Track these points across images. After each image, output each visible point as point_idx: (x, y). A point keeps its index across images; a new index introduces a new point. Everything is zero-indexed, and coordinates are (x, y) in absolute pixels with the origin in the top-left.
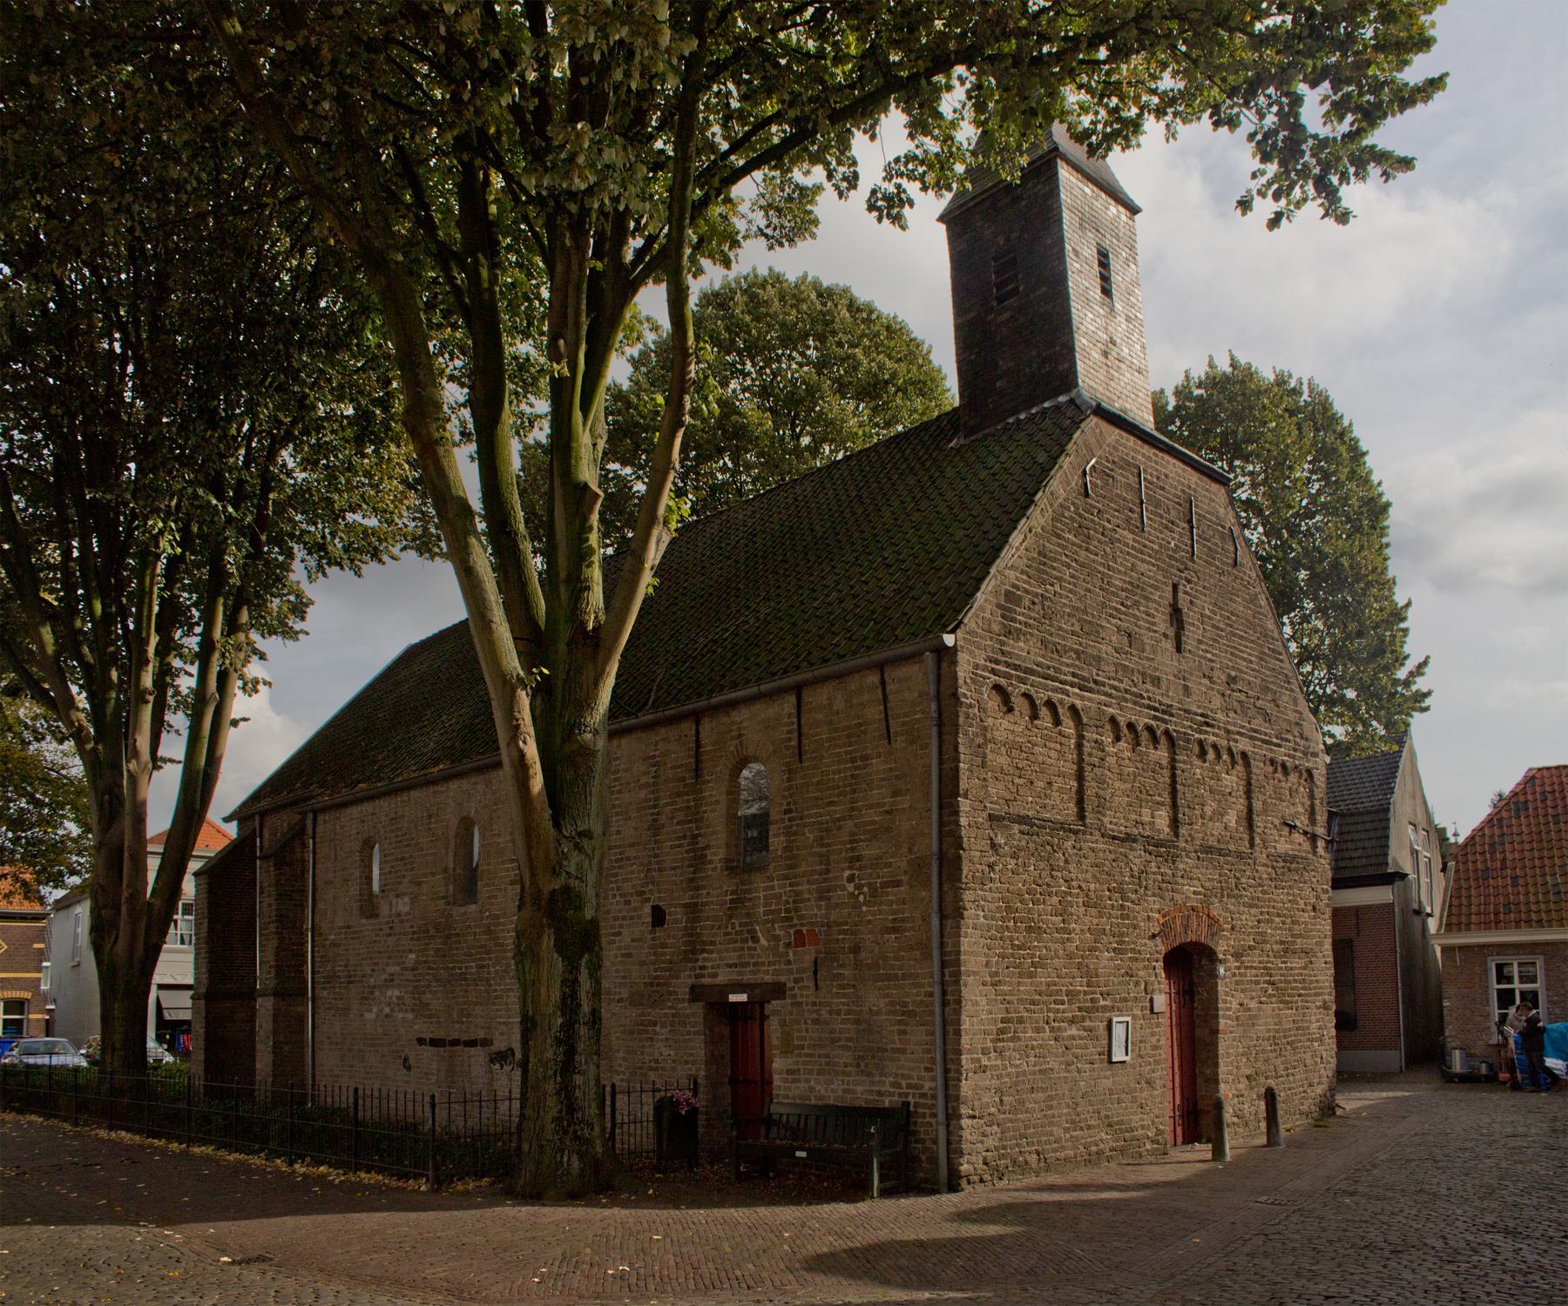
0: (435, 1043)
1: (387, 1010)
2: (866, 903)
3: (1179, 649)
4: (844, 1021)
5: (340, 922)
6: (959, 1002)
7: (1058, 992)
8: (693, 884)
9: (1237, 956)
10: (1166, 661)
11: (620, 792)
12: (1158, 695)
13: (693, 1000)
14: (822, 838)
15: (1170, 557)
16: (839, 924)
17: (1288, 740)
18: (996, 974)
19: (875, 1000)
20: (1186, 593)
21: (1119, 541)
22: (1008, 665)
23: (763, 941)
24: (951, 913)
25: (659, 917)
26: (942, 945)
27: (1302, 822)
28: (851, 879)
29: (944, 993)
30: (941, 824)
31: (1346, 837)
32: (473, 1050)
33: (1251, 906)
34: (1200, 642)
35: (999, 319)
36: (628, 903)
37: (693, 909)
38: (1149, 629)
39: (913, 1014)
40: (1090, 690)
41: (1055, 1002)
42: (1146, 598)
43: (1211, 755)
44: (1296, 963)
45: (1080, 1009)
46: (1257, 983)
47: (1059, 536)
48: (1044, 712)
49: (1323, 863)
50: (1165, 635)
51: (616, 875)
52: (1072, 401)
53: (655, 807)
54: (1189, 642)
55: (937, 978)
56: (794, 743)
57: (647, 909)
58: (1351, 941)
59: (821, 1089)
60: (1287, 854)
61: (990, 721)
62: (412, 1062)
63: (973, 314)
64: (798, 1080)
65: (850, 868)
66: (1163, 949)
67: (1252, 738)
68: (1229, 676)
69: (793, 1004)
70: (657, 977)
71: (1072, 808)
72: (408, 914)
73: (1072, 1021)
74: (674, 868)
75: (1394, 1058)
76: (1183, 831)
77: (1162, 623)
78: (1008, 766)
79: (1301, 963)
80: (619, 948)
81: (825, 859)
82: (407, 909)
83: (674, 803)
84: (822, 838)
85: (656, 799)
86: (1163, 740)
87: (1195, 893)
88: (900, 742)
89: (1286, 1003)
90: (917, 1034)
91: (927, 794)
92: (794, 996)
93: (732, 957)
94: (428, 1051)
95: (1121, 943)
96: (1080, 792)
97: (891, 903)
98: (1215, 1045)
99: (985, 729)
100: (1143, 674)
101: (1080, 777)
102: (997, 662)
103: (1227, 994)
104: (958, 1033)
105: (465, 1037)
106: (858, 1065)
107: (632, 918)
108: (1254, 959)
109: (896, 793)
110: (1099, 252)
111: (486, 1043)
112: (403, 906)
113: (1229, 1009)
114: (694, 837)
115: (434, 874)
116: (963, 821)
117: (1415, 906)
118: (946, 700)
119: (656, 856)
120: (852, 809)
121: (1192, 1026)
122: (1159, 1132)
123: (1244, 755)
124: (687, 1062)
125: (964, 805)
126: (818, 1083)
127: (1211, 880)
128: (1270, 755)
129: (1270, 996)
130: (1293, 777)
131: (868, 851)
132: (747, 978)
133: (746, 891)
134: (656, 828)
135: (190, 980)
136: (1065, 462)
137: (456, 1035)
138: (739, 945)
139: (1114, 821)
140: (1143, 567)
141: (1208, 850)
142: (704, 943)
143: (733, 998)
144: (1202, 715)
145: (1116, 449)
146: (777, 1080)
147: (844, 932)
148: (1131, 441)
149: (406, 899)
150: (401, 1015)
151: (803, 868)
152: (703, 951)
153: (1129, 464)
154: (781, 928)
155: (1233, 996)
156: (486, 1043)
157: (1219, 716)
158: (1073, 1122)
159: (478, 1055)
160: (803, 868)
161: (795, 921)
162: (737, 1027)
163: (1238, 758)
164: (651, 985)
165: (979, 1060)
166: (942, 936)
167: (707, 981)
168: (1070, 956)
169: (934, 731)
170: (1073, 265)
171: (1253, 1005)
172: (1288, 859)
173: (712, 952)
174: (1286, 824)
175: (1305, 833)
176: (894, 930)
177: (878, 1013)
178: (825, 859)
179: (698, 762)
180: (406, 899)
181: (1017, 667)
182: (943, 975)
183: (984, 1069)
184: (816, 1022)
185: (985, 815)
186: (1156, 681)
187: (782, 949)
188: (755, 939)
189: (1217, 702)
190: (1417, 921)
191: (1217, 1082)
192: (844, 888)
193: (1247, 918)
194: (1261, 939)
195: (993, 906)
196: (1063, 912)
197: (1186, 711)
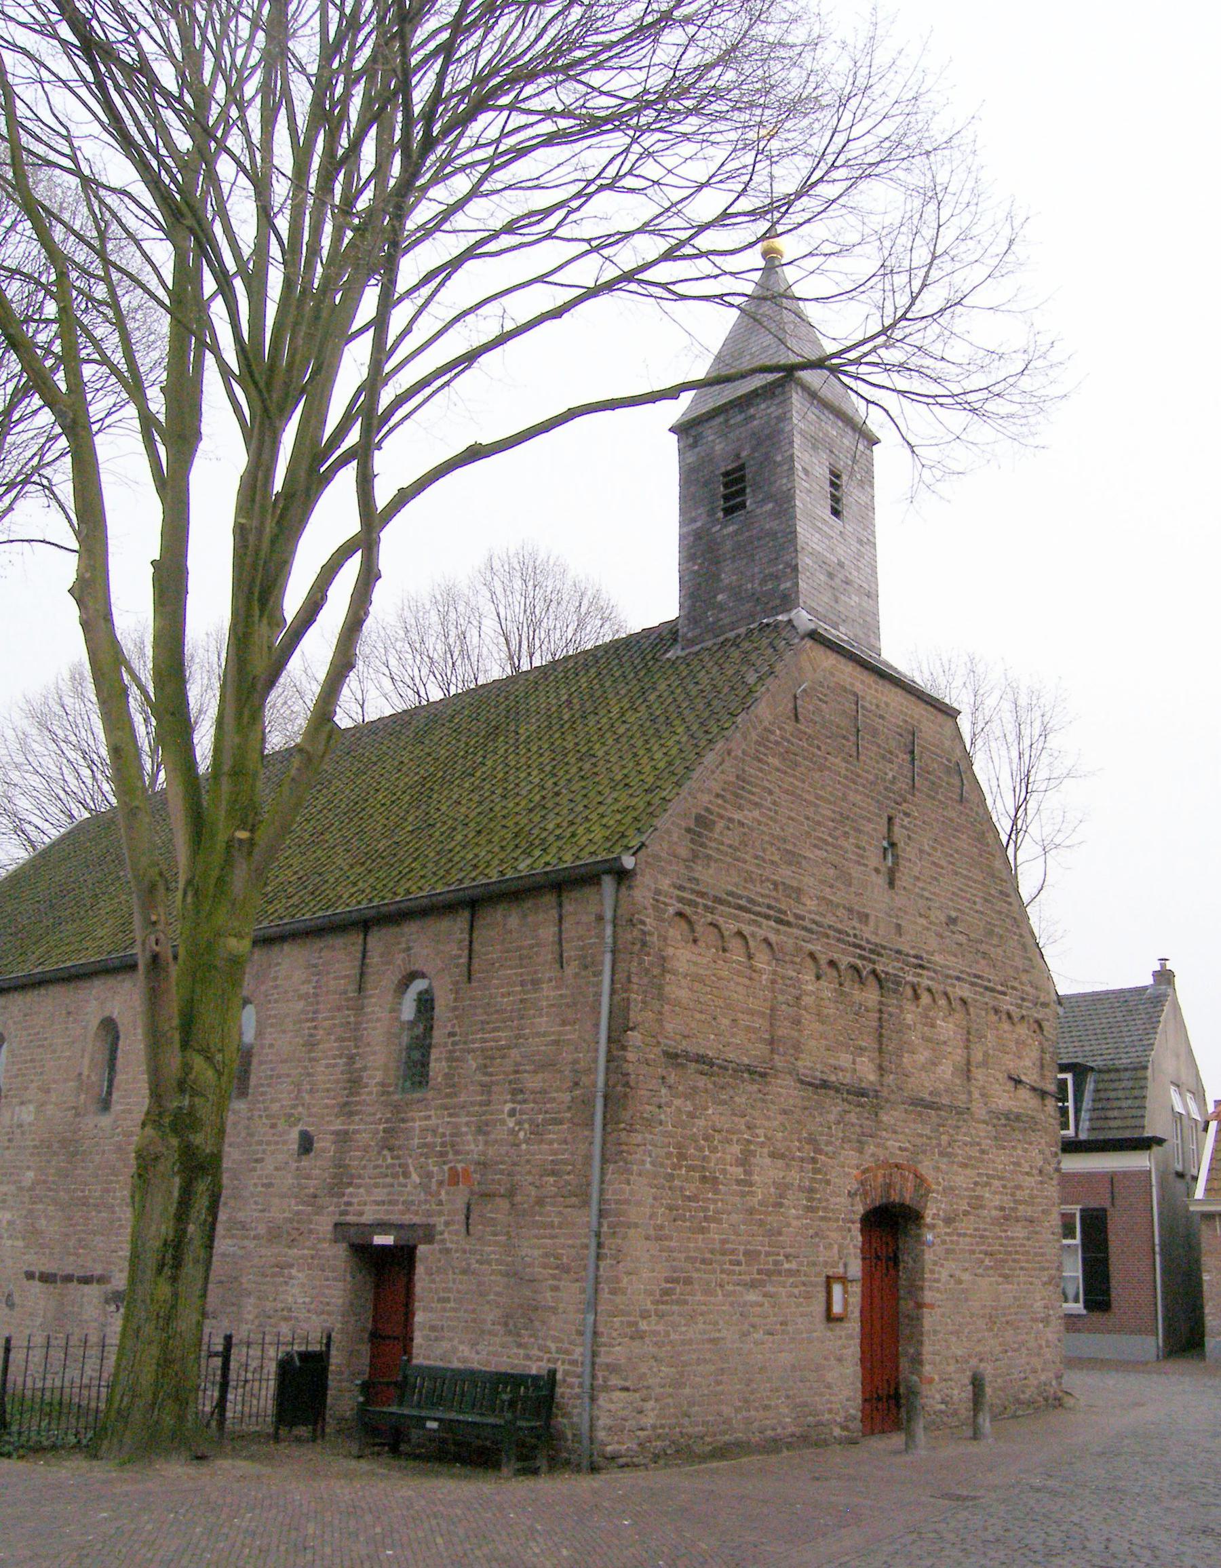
0: (46, 1278)
2: (527, 1141)
3: (891, 884)
4: (493, 1272)
7: (733, 1252)
8: (347, 1110)
9: (948, 1221)
10: (877, 898)
11: (276, 1001)
12: (867, 932)
14: (486, 1066)
15: (886, 789)
16: (497, 1163)
17: (1013, 988)
18: (661, 1227)
20: (903, 827)
21: (829, 769)
22: (693, 891)
23: (415, 1178)
25: (306, 1144)
26: (602, 1192)
28: (512, 1113)
29: (600, 1245)
31: (1102, 1095)
33: (965, 1166)
34: (917, 879)
35: (725, 532)
36: (273, 1126)
37: (343, 1138)
38: (859, 863)
39: (566, 1269)
40: (788, 924)
41: (731, 1263)
42: (857, 830)
43: (925, 999)
44: (1018, 1232)
45: (760, 1272)
46: (972, 1252)
47: (760, 761)
50: (877, 870)
51: (263, 1094)
52: (790, 621)
53: (313, 1020)
54: (903, 880)
55: (595, 1227)
56: (464, 960)
57: (294, 1134)
58: (1104, 1210)
59: (465, 1350)
60: (1010, 1112)
61: (670, 951)
62: (17, 1299)
63: (699, 524)
64: (452, 1333)
65: (513, 1101)
66: (860, 1209)
67: (973, 984)
68: (949, 917)
69: (441, 1251)
70: (298, 1213)
72: (30, 1124)
73: (753, 1285)
74: (328, 1090)
75: (1152, 1344)
80: (259, 1177)
82: (32, 1118)
83: (333, 1018)
84: (486, 1066)
85: (315, 1012)
87: (900, 1148)
88: (571, 970)
89: (1006, 1276)
91: (597, 1025)
92: (443, 1241)
93: (380, 1194)
94: (37, 1286)
95: (810, 1199)
97: (551, 1143)
98: (919, 1318)
99: (664, 958)
100: (850, 910)
102: (681, 888)
103: (935, 1263)
105: (80, 1273)
106: (506, 1324)
107: (277, 1143)
108: (966, 1225)
109: (564, 1023)
110: (832, 473)
111: (101, 1280)
113: (937, 1280)
114: (351, 1058)
115: (66, 1080)
117: (1179, 1168)
119: (309, 1075)
120: (518, 1037)
123: (964, 1001)
124: (323, 1313)
126: (461, 1342)
127: (921, 1136)
128: (992, 1003)
129: (987, 1268)
131: (533, 1082)
132: (395, 1218)
133: (403, 1120)
134: (311, 1045)
137: (69, 1270)
138: (388, 1180)
139: (810, 1063)
140: (852, 796)
141: (917, 1102)
142: (352, 1176)
143: (379, 1240)
144: (916, 957)
145: (832, 674)
147: (502, 1172)
148: (858, 672)
149: (31, 1107)
150: (9, 1243)
151: (463, 1098)
152: (350, 1184)
153: (845, 690)
154: (436, 1164)
155: (945, 1265)
156: (101, 1280)
157: (937, 958)
158: (746, 1401)
159: (93, 1290)
160: (463, 1098)
161: (451, 1156)
162: (386, 1270)
163: (956, 1004)
164: (291, 1220)
165: (636, 1323)
166: (602, 1182)
167: (350, 1219)
168: (751, 1211)
169: (608, 958)
170: (802, 484)
171: (966, 1276)
172: (1012, 1118)
173: (359, 1186)
174: (1010, 1078)
175: (1033, 1089)
176: (553, 1173)
177: (531, 1265)
179: (362, 974)
180: (31, 1107)
181: (702, 895)
182: (600, 1225)
183: (639, 1336)
185: (657, 1050)
186: (863, 918)
187: (434, 1187)
188: (406, 1175)
189: (933, 943)
190: (1180, 1185)
191: (921, 1363)
192: (503, 1122)
193: (962, 1179)
194: (977, 1204)
195: (662, 1152)
196: (744, 1161)
197: (898, 952)
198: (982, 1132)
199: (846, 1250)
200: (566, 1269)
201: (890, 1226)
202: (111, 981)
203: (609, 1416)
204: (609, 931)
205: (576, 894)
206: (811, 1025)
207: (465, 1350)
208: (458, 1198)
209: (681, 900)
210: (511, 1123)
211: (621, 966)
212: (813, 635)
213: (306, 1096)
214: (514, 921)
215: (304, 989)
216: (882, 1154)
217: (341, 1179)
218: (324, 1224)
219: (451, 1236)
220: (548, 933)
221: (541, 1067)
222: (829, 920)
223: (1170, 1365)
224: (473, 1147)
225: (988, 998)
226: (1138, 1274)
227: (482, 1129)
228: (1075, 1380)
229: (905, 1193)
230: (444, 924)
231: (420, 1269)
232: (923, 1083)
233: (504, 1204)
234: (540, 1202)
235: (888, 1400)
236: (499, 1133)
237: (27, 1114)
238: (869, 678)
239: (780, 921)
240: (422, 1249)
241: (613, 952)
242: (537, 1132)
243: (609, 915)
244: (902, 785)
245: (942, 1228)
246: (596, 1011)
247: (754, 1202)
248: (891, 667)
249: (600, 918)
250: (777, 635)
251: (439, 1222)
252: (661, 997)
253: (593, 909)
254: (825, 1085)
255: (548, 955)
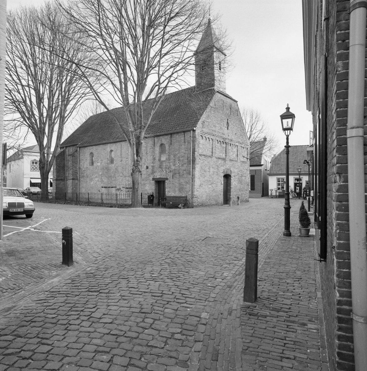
1: (95, 182)
3: (228, 129)
5: (85, 167)
6: (194, 181)
9: (234, 176)
13: (153, 180)
19: (182, 181)
24: (194, 168)
25: (147, 168)
27: (246, 156)
28: (179, 163)
30: (193, 155)
32: (113, 189)
43: (232, 145)
48: (208, 139)
49: (249, 163)
54: (229, 128)
56: (170, 142)
57: (145, 166)
71: (211, 153)
73: (210, 185)
75: (260, 195)
76: (227, 157)
77: (226, 125)
78: (203, 146)
79: (244, 178)
81: (175, 160)
86: (225, 143)
88: (186, 143)
90: (188, 185)
91: (190, 151)
93: (159, 174)
94: (104, 189)
96: (212, 151)
98: (230, 190)
101: (212, 149)
104: (194, 185)
108: (237, 177)
109: (186, 151)
111: (115, 187)
112: (99, 164)
116: (196, 155)
118: (194, 137)
121: (227, 187)
122: (222, 202)
125: (196, 153)
130: (245, 149)
131: (181, 159)
135: (40, 177)
136: (212, 100)
146: (166, 193)
148: (222, 96)
156: (115, 187)
159: (114, 189)
162: (160, 183)
163: (236, 146)
167: (155, 177)
168: (210, 175)
172: (243, 162)
176: (185, 171)
178: (175, 160)
181: (204, 133)
184: (173, 184)
186: (224, 134)
193: (236, 171)
198: (239, 164)
199: (222, 179)
200: (188, 183)
201: (227, 177)
202: (111, 144)
203: (196, 201)
204: (192, 138)
205: (187, 133)
206: (217, 149)
207: (173, 194)
208: (171, 174)
209: (201, 134)
210: (179, 164)
211: (194, 143)
212: (218, 92)
213: (147, 161)
214: (177, 137)
215: (145, 146)
216: (226, 167)
217: (153, 172)
218: (151, 178)
219: (171, 179)
220: (183, 138)
221: (183, 157)
222: (220, 135)
223: (262, 198)
224: (173, 167)
225: (240, 145)
226: (259, 186)
227: (174, 165)
228: (250, 199)
229: (229, 173)
230: (166, 137)
231: (166, 184)
232: (232, 158)
233: (178, 175)
234: (183, 174)
235: (227, 200)
236: (177, 165)
237: (99, 164)
238: (225, 97)
239: (213, 136)
240: (166, 181)
241: (193, 141)
242: (182, 165)
243: (192, 136)
244: (229, 114)
245: (234, 177)
246: (190, 149)
247: (210, 174)
248: (228, 95)
249: (190, 136)
250: (212, 92)
251: (168, 177)
252: (199, 147)
253: (189, 135)
254: (219, 158)
255: (183, 141)
